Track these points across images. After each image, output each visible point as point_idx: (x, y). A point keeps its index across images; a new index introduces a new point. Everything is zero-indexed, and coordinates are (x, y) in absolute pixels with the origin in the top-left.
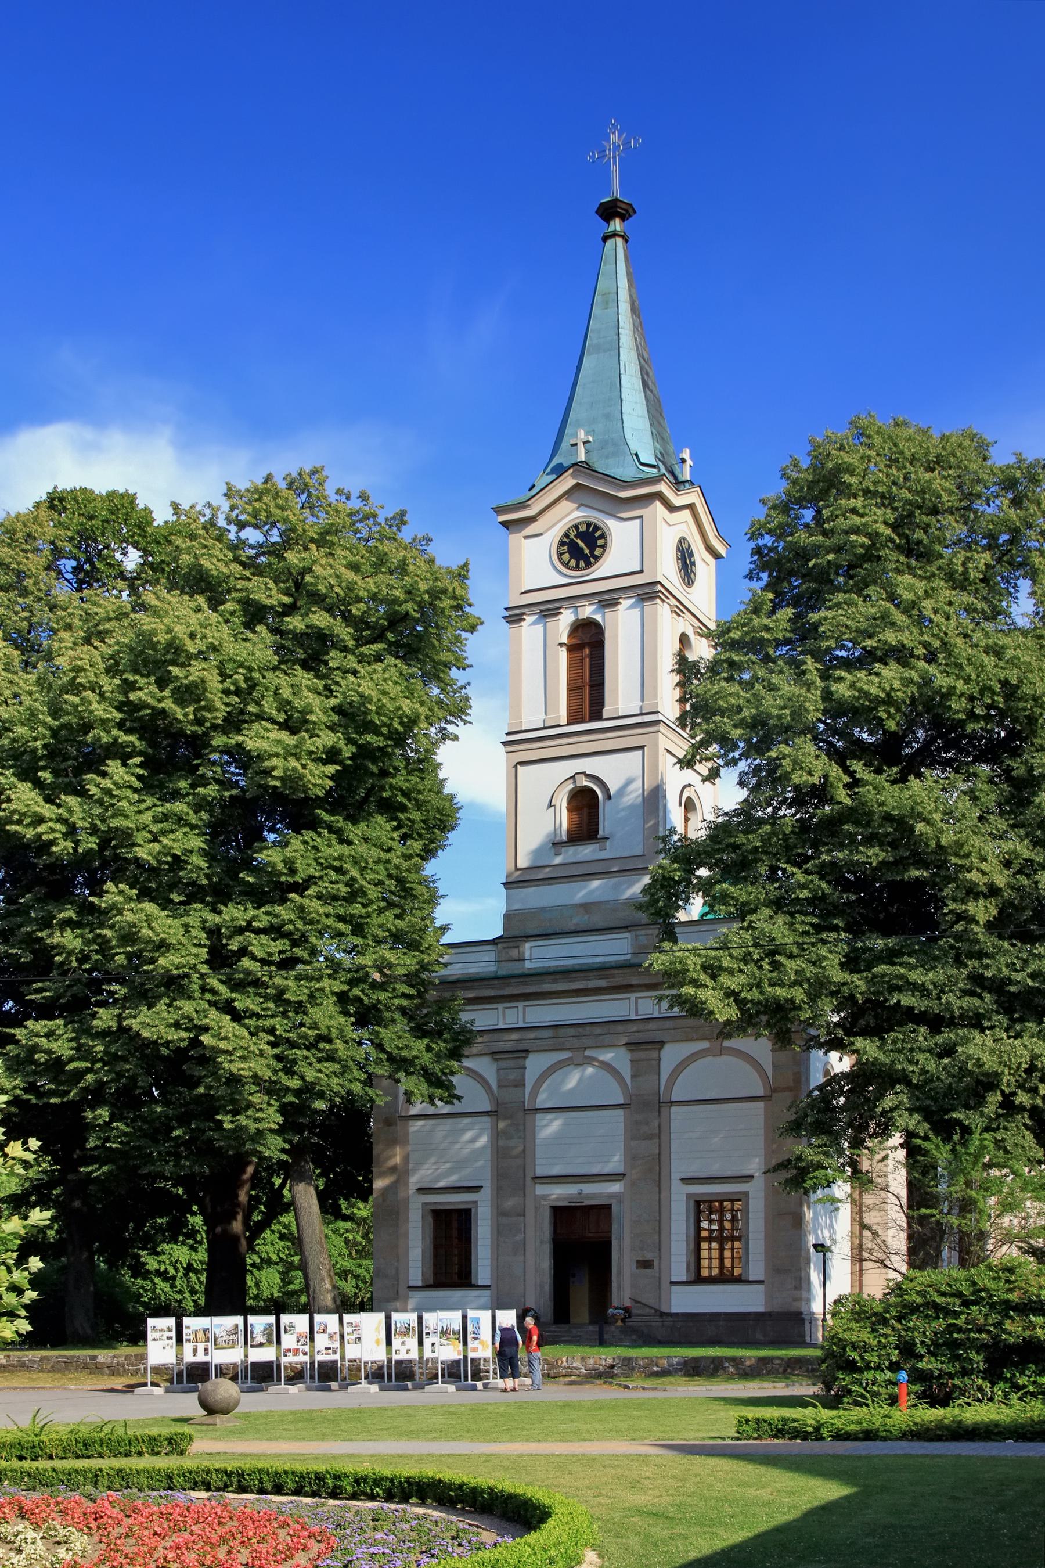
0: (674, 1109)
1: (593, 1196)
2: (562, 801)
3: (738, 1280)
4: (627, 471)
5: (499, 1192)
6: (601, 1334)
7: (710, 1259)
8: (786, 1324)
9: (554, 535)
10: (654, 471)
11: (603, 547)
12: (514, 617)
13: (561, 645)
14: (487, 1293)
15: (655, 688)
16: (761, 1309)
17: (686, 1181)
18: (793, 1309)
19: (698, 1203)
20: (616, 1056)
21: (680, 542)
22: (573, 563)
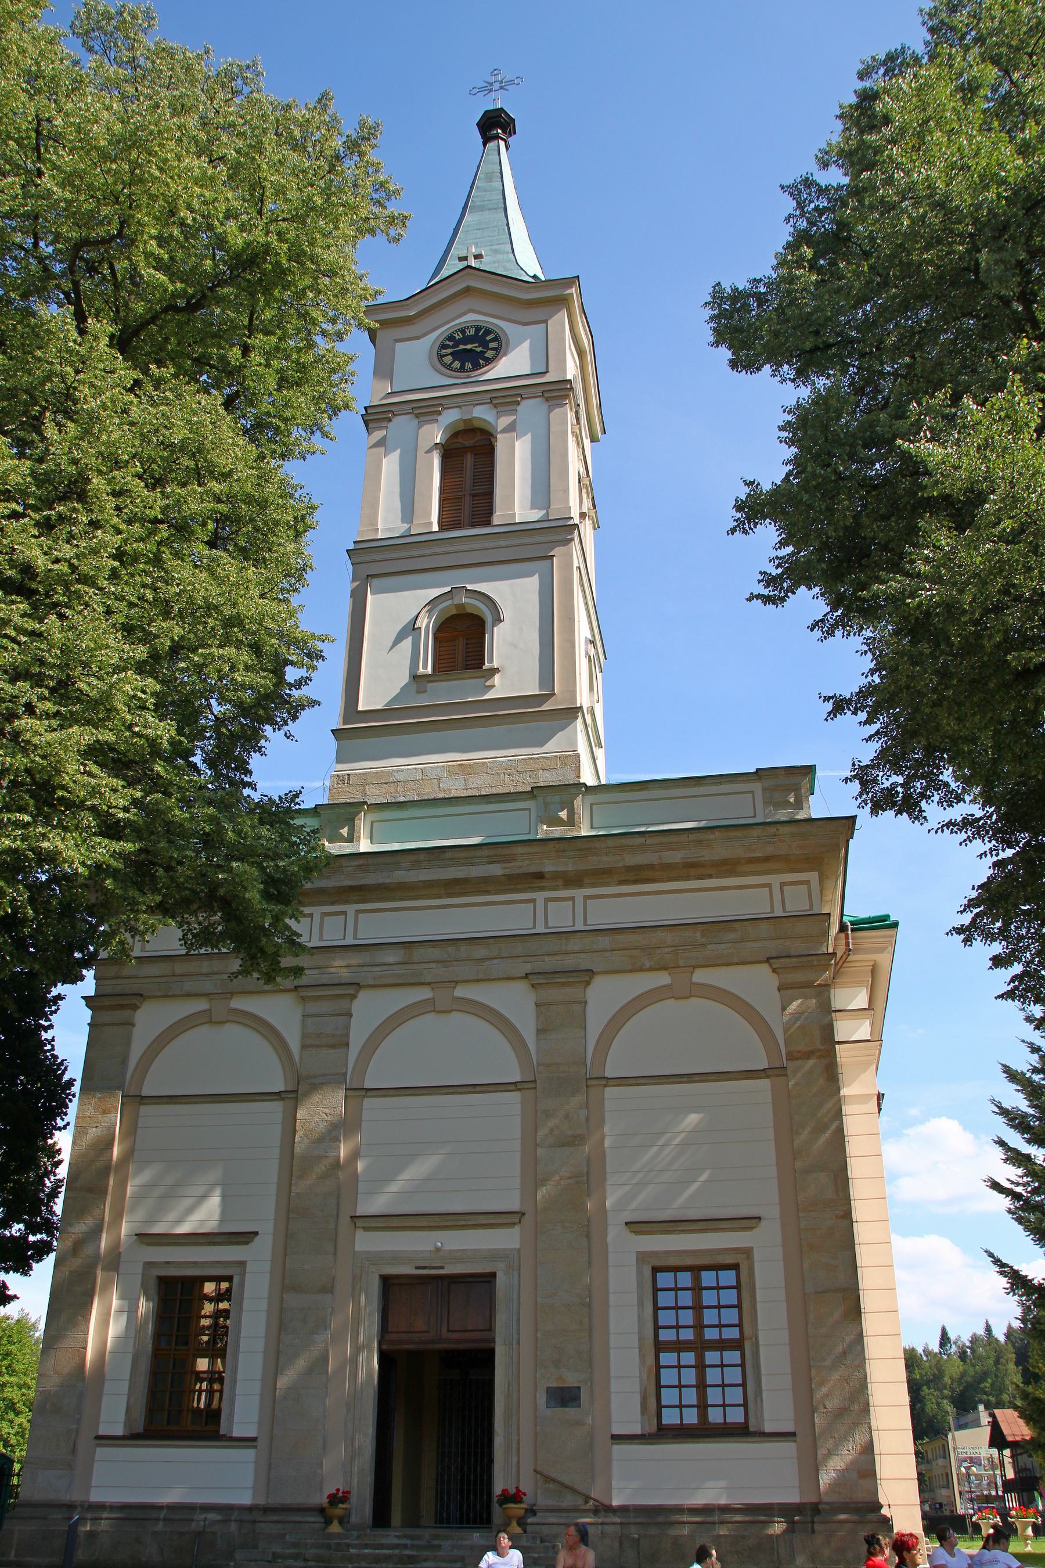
0: (610, 1092)
1: (456, 1256)
3: (741, 1431)
5: (287, 1241)
17: (636, 1226)
18: (860, 1496)
20: (516, 1001)
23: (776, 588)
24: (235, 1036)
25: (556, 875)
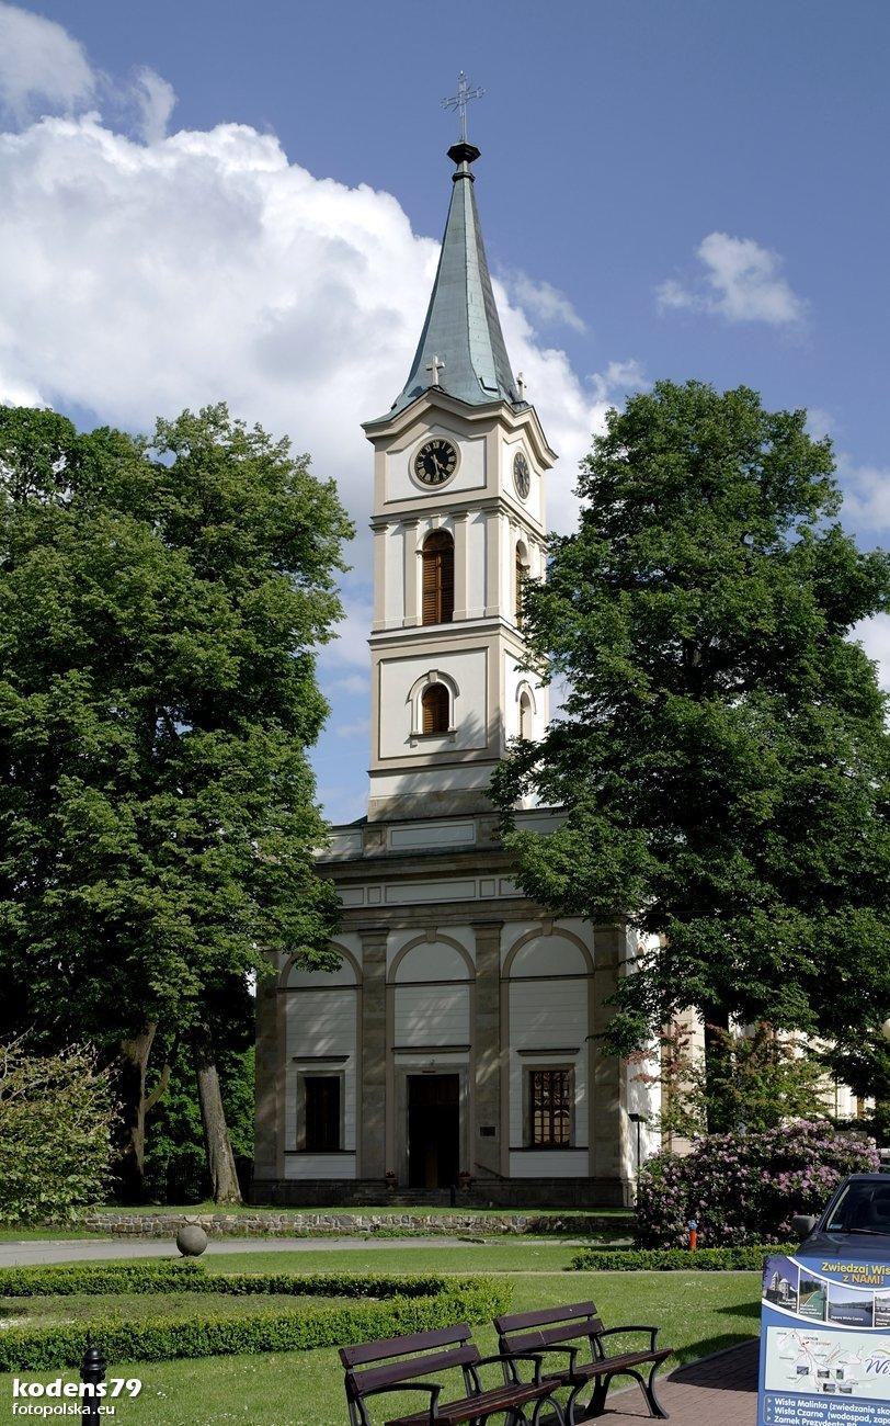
0: (397, 990)
2: (418, 696)
4: (474, 397)
5: (362, 1062)
6: (453, 1196)
7: (543, 1126)
8: (607, 1185)
9: (412, 451)
10: (495, 394)
11: (454, 463)
12: (379, 525)
13: (418, 552)
14: (353, 1158)
15: (497, 593)
16: (585, 1174)
17: (522, 1052)
18: (612, 1175)
19: (532, 1074)
20: (465, 936)
21: (516, 457)
22: (428, 477)
23: (323, 728)
24: (441, 948)
25: (484, 869)
